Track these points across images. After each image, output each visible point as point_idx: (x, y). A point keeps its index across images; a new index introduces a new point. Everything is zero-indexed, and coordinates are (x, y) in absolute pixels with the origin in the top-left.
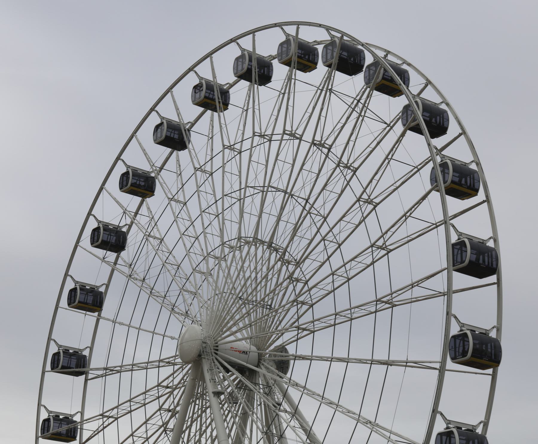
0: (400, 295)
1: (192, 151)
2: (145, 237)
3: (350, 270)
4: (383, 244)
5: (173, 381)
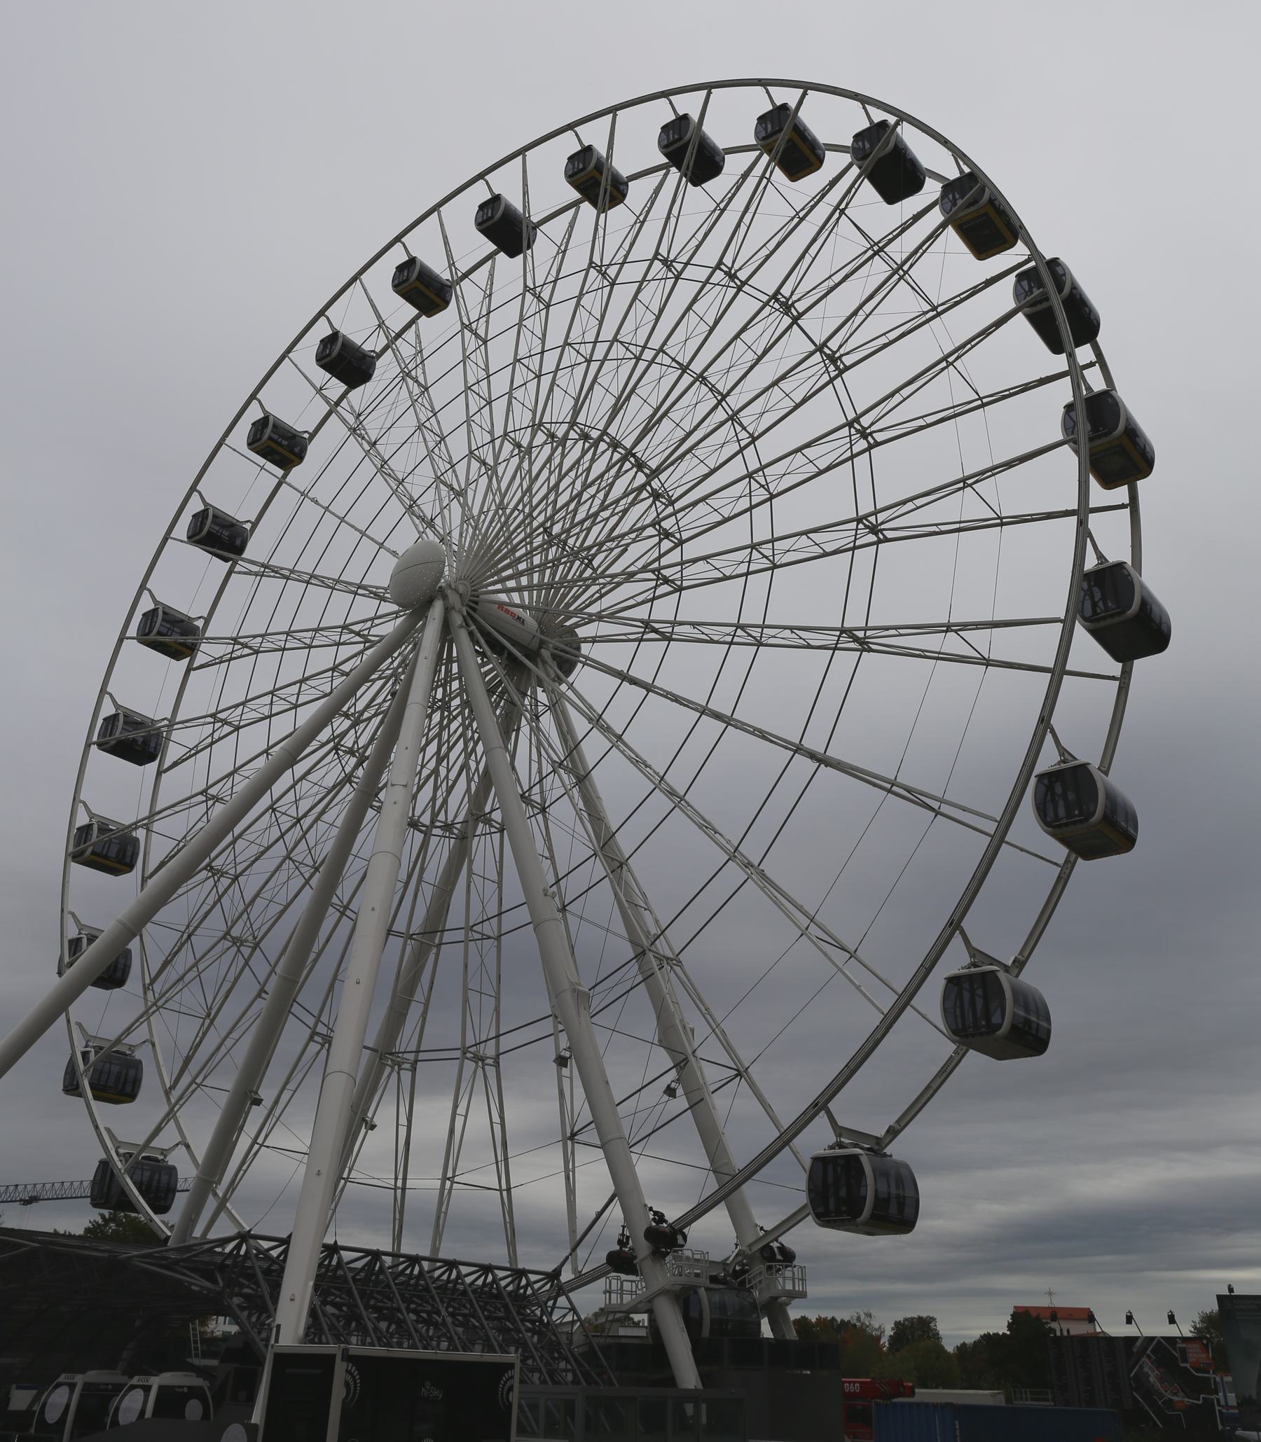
0: (901, 635)
1: (529, 258)
2: (401, 375)
3: (742, 562)
5: (370, 629)
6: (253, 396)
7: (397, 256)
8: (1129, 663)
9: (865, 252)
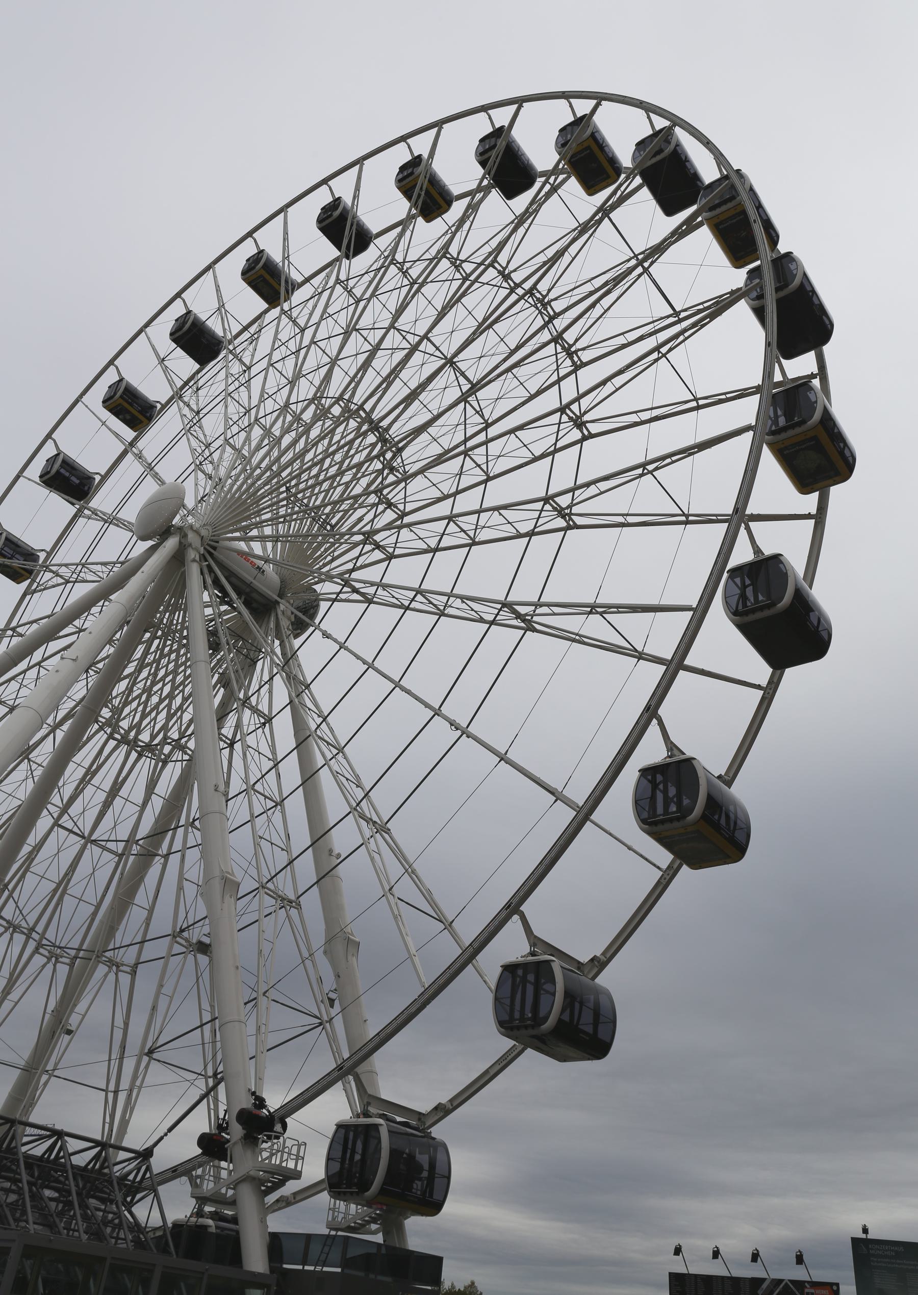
0: (555, 614)
4: (567, 508)
6: (49, 436)
7: (248, 250)
8: (779, 672)
9: (628, 260)
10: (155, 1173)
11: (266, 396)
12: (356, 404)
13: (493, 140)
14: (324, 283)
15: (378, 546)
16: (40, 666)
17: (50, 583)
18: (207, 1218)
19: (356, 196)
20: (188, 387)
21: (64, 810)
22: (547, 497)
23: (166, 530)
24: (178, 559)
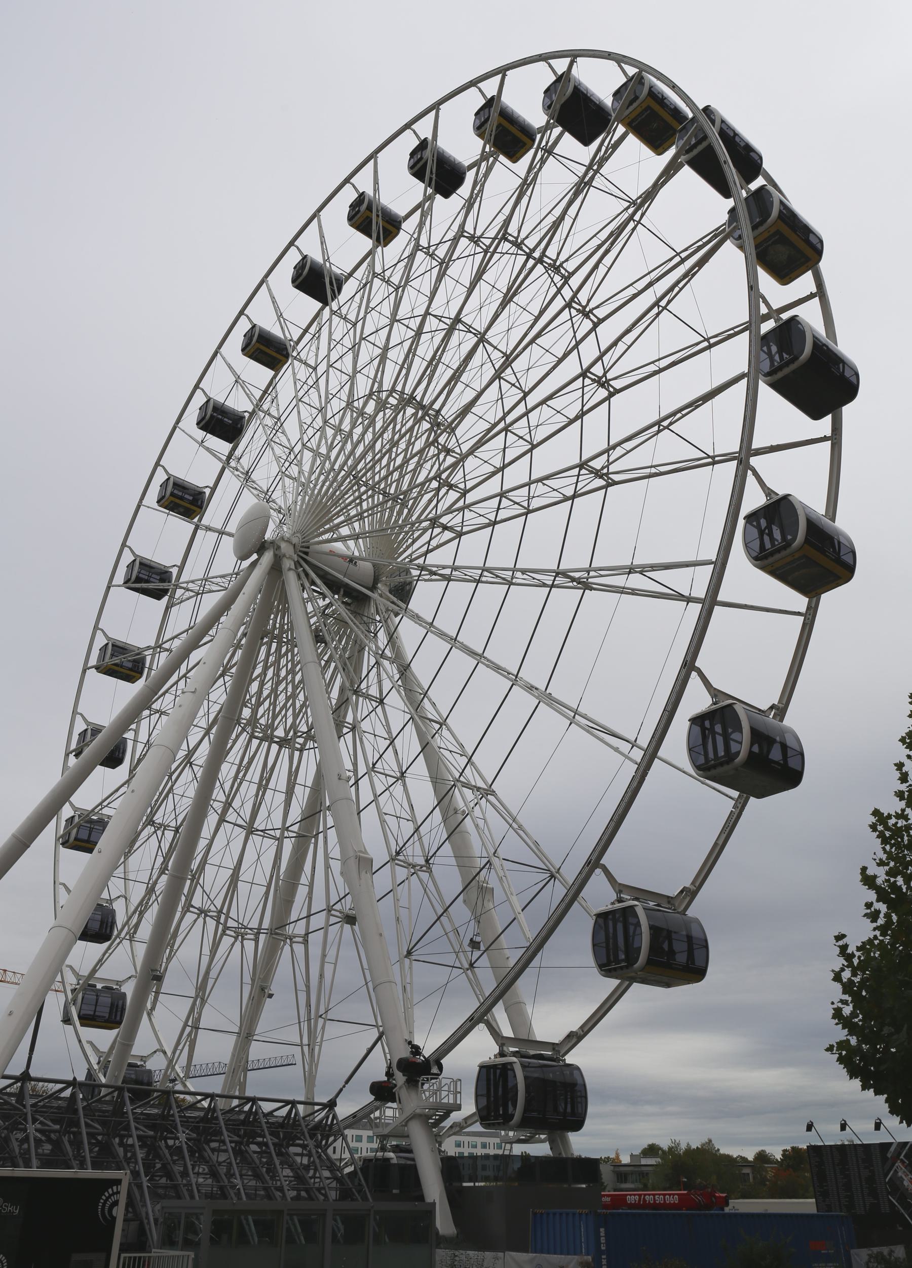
4: (603, 468)
6: (157, 464)
7: (293, 258)
10: (340, 1119)
11: (331, 397)
12: (407, 395)
13: (487, 110)
14: (366, 273)
15: (445, 528)
16: (186, 678)
17: (185, 597)
18: (389, 1152)
19: (376, 189)
20: (267, 395)
21: (228, 805)
22: (581, 463)
23: (260, 547)
24: (276, 569)
